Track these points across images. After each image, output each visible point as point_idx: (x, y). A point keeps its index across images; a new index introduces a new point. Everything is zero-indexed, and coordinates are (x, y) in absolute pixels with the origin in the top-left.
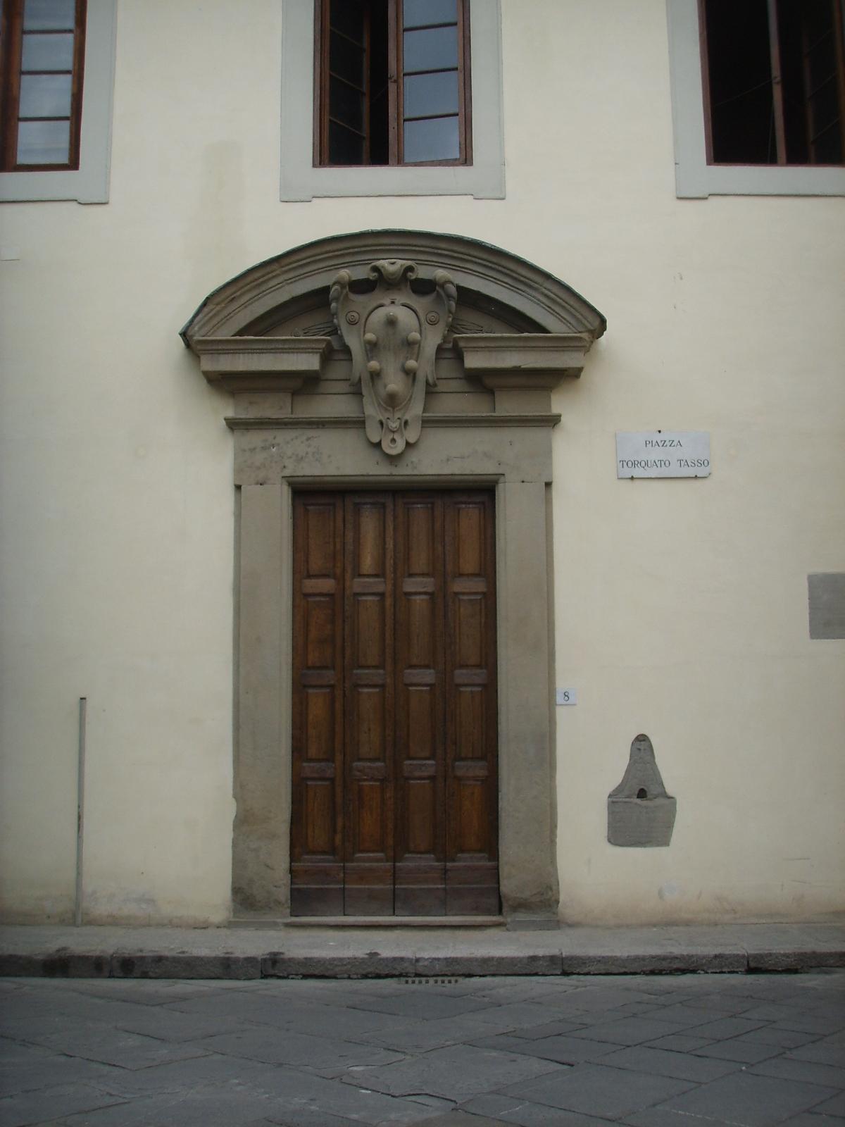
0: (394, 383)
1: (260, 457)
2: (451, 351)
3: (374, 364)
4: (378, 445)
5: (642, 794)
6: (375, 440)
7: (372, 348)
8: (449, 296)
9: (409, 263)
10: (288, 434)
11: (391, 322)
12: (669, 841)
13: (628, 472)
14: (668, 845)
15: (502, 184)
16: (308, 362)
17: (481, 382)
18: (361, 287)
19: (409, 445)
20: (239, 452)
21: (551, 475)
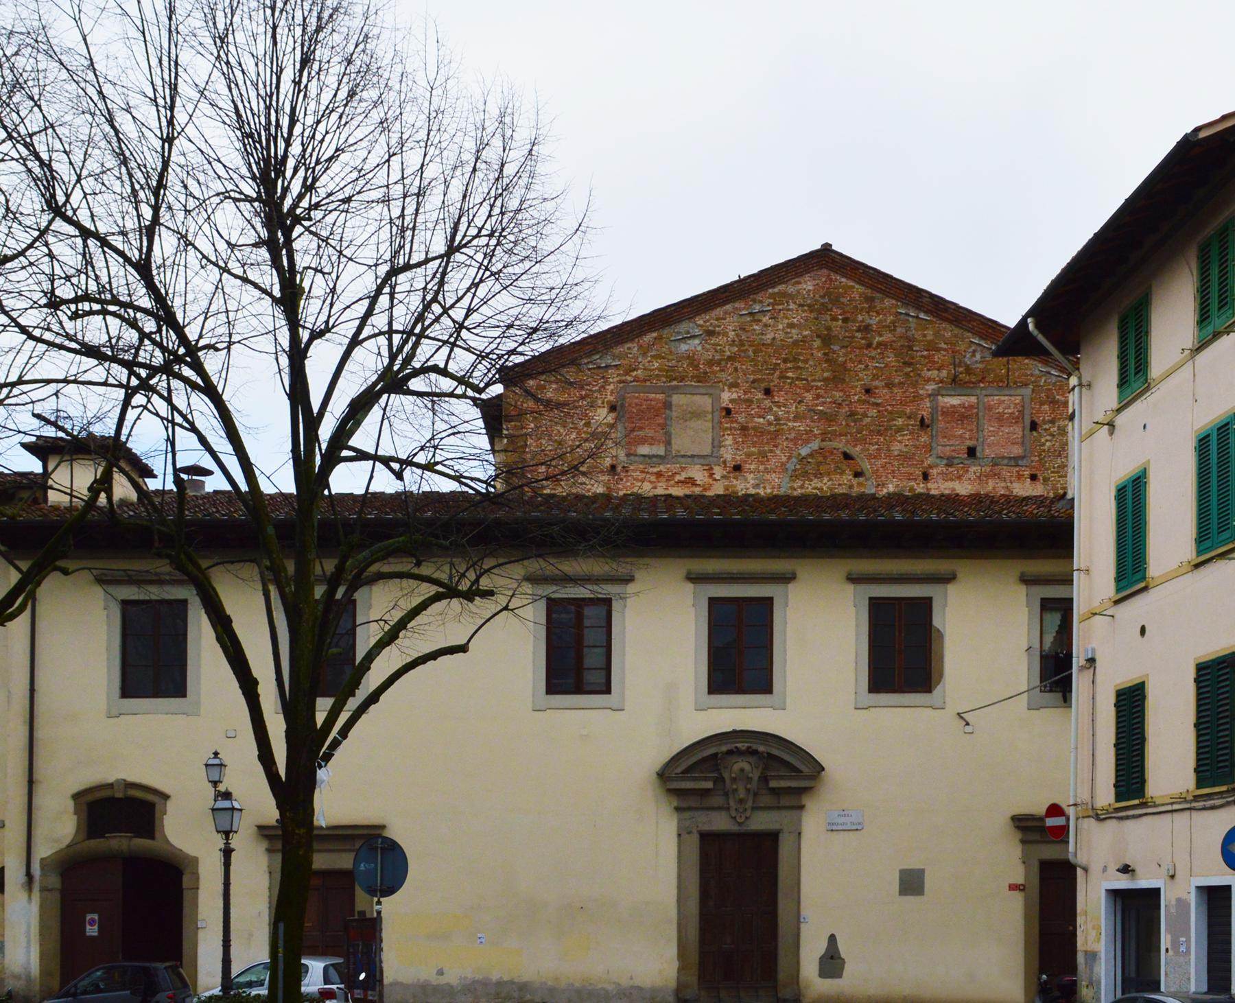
0: (742, 794)
1: (687, 823)
2: (764, 779)
3: (735, 787)
4: (735, 818)
5: (832, 958)
6: (733, 815)
7: (734, 780)
8: (764, 757)
9: (749, 745)
10: (700, 813)
11: (742, 770)
12: (842, 974)
13: (830, 828)
14: (923, 895)
15: (785, 702)
16: (709, 785)
17: (776, 792)
18: (730, 752)
19: (747, 818)
20: (680, 821)
21: (801, 829)
